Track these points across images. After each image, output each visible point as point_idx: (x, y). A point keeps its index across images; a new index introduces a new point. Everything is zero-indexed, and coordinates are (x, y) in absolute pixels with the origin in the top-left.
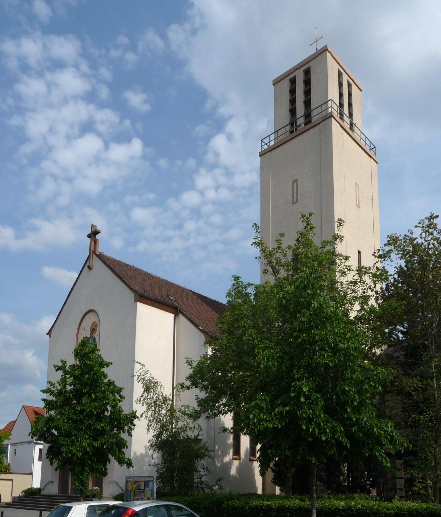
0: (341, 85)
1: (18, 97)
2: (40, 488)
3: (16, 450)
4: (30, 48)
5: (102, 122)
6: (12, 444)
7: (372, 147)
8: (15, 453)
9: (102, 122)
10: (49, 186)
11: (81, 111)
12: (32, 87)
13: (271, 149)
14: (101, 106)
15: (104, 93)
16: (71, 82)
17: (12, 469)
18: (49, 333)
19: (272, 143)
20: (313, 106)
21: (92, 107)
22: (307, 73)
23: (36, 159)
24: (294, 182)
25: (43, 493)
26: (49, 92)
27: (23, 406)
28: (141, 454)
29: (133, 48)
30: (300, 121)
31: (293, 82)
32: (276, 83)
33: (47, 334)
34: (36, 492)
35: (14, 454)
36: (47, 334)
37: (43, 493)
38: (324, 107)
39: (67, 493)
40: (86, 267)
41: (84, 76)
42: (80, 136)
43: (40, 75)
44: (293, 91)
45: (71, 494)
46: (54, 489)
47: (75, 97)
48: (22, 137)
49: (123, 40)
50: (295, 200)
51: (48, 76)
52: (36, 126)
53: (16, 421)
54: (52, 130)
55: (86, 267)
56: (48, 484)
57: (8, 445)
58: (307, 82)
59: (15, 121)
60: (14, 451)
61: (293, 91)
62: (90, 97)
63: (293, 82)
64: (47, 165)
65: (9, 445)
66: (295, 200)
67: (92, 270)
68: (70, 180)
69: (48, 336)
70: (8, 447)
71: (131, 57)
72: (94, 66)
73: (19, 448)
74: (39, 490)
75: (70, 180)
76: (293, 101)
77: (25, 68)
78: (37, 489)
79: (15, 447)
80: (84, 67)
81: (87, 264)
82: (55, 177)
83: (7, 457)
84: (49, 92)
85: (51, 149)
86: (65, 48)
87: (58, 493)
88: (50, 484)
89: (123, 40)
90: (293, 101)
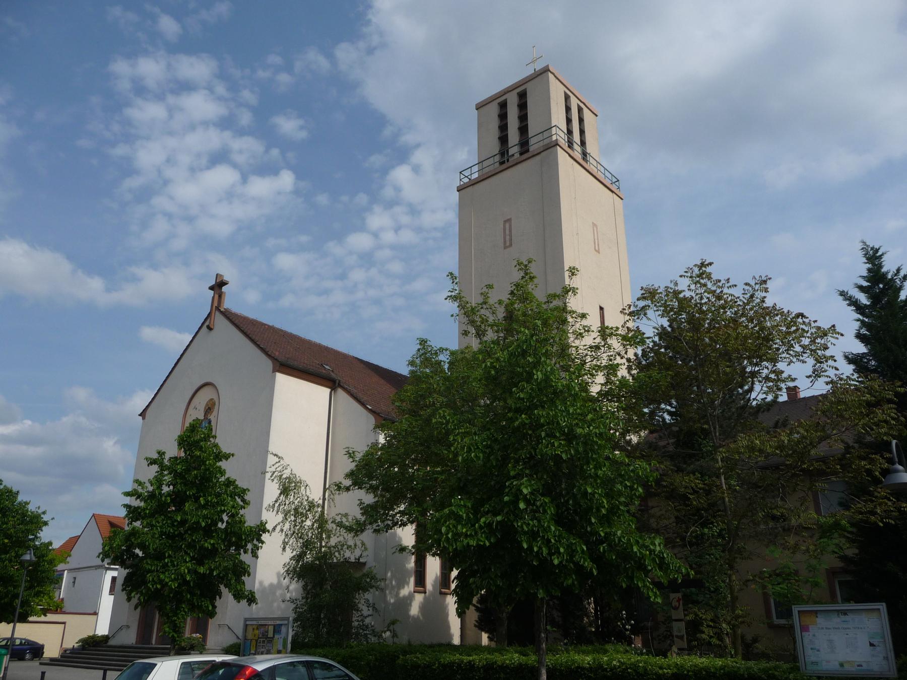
0: (568, 109)
2: (107, 636)
4: (150, 69)
5: (241, 152)
6: (70, 570)
7: (614, 180)
8: (74, 582)
10: (160, 227)
11: (214, 139)
12: (149, 112)
13: (473, 183)
14: (241, 132)
15: (246, 118)
17: (67, 607)
19: (475, 176)
20: (531, 132)
21: (227, 134)
22: (523, 96)
23: (145, 194)
24: (505, 222)
25: (112, 642)
26: (171, 117)
28: (271, 585)
30: (514, 150)
31: (503, 106)
32: (479, 107)
34: (101, 641)
37: (112, 642)
38: (546, 135)
39: (149, 642)
41: (220, 99)
42: (208, 168)
43: (160, 97)
44: (503, 116)
47: (206, 124)
48: (128, 169)
50: (508, 244)
51: (171, 99)
52: (149, 156)
56: (121, 628)
58: (523, 107)
59: (120, 150)
61: (503, 116)
62: (226, 123)
63: (503, 106)
64: (159, 202)
66: (508, 244)
68: (190, 219)
70: (63, 574)
71: (284, 78)
74: (106, 638)
75: (190, 219)
76: (503, 128)
77: (140, 89)
79: (74, 574)
80: (221, 89)
82: (169, 216)
84: (171, 117)
86: (196, 68)
90: (503, 128)
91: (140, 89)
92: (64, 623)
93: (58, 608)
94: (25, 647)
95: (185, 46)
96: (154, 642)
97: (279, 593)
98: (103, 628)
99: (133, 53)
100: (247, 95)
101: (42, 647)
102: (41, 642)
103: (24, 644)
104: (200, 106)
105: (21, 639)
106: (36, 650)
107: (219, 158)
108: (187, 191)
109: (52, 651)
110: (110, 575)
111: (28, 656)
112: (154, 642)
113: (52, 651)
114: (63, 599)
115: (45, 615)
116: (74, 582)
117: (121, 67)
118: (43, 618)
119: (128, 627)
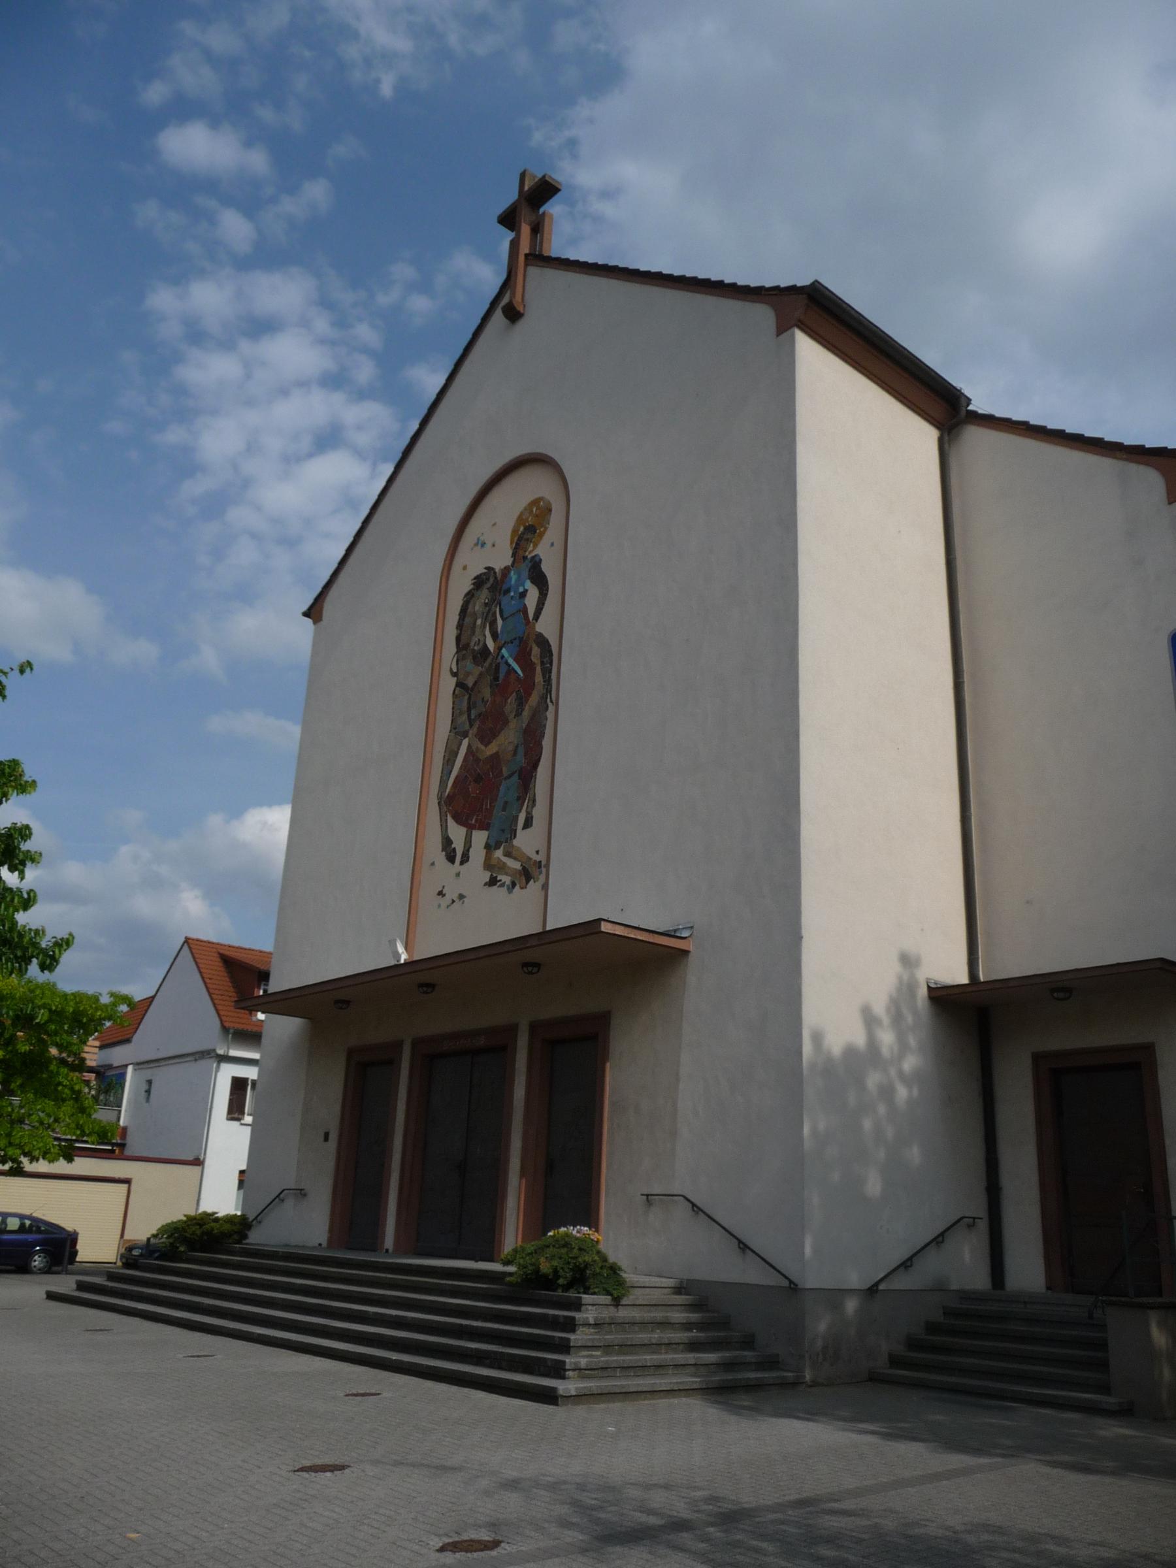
1: (181, 391)
2: (243, 1217)
3: (150, 1082)
4: (210, 298)
5: (359, 428)
6: (139, 1065)
8: (148, 1092)
9: (359, 428)
10: (245, 554)
11: (319, 407)
12: (212, 370)
14: (362, 395)
15: (365, 372)
16: (294, 353)
17: (134, 1145)
18: (314, 612)
21: (338, 398)
23: (215, 505)
25: (256, 1238)
26: (248, 376)
27: (187, 941)
28: (850, 1052)
29: (424, 286)
33: (306, 614)
34: (229, 1235)
35: (143, 1094)
36: (306, 614)
37: (256, 1238)
39: (374, 1244)
40: (498, 314)
41: (322, 341)
42: (310, 455)
43: (227, 345)
45: (399, 1249)
46: (308, 1226)
47: (303, 384)
48: (187, 464)
49: (403, 271)
51: (245, 345)
52: (218, 441)
53: (153, 998)
54: (252, 448)
55: (498, 314)
56: (279, 1198)
57: (126, 1066)
59: (174, 435)
60: (145, 1087)
62: (334, 381)
64: (238, 515)
65: (130, 1068)
67: (521, 325)
68: (289, 542)
69: (309, 621)
70: (123, 1076)
71: (420, 304)
72: (341, 323)
73: (163, 1077)
74: (239, 1226)
75: (289, 542)
77: (196, 335)
78: (230, 1219)
79: (148, 1074)
80: (322, 324)
81: (505, 300)
82: (254, 536)
83: (120, 1106)
84: (248, 376)
85: (247, 483)
86: (283, 292)
87: (331, 1244)
88: (289, 1203)
89: (403, 271)
91: (196, 335)
92: (127, 1181)
93: (113, 1144)
94: (30, 1237)
95: (265, 257)
96: (389, 1242)
97: (873, 1080)
98: (220, 1197)
99: (181, 272)
100: (366, 333)
101: (73, 1238)
102: (69, 1226)
103: (29, 1230)
104: (294, 353)
105: (22, 1217)
106: (58, 1246)
107: (328, 439)
108: (284, 496)
109: (98, 1246)
110: (226, 1075)
111: (38, 1261)
112: (389, 1242)
113: (98, 1246)
114: (125, 1129)
115: (70, 1159)
116: (148, 1092)
117: (163, 299)
118: (61, 1167)
119: (301, 1193)
